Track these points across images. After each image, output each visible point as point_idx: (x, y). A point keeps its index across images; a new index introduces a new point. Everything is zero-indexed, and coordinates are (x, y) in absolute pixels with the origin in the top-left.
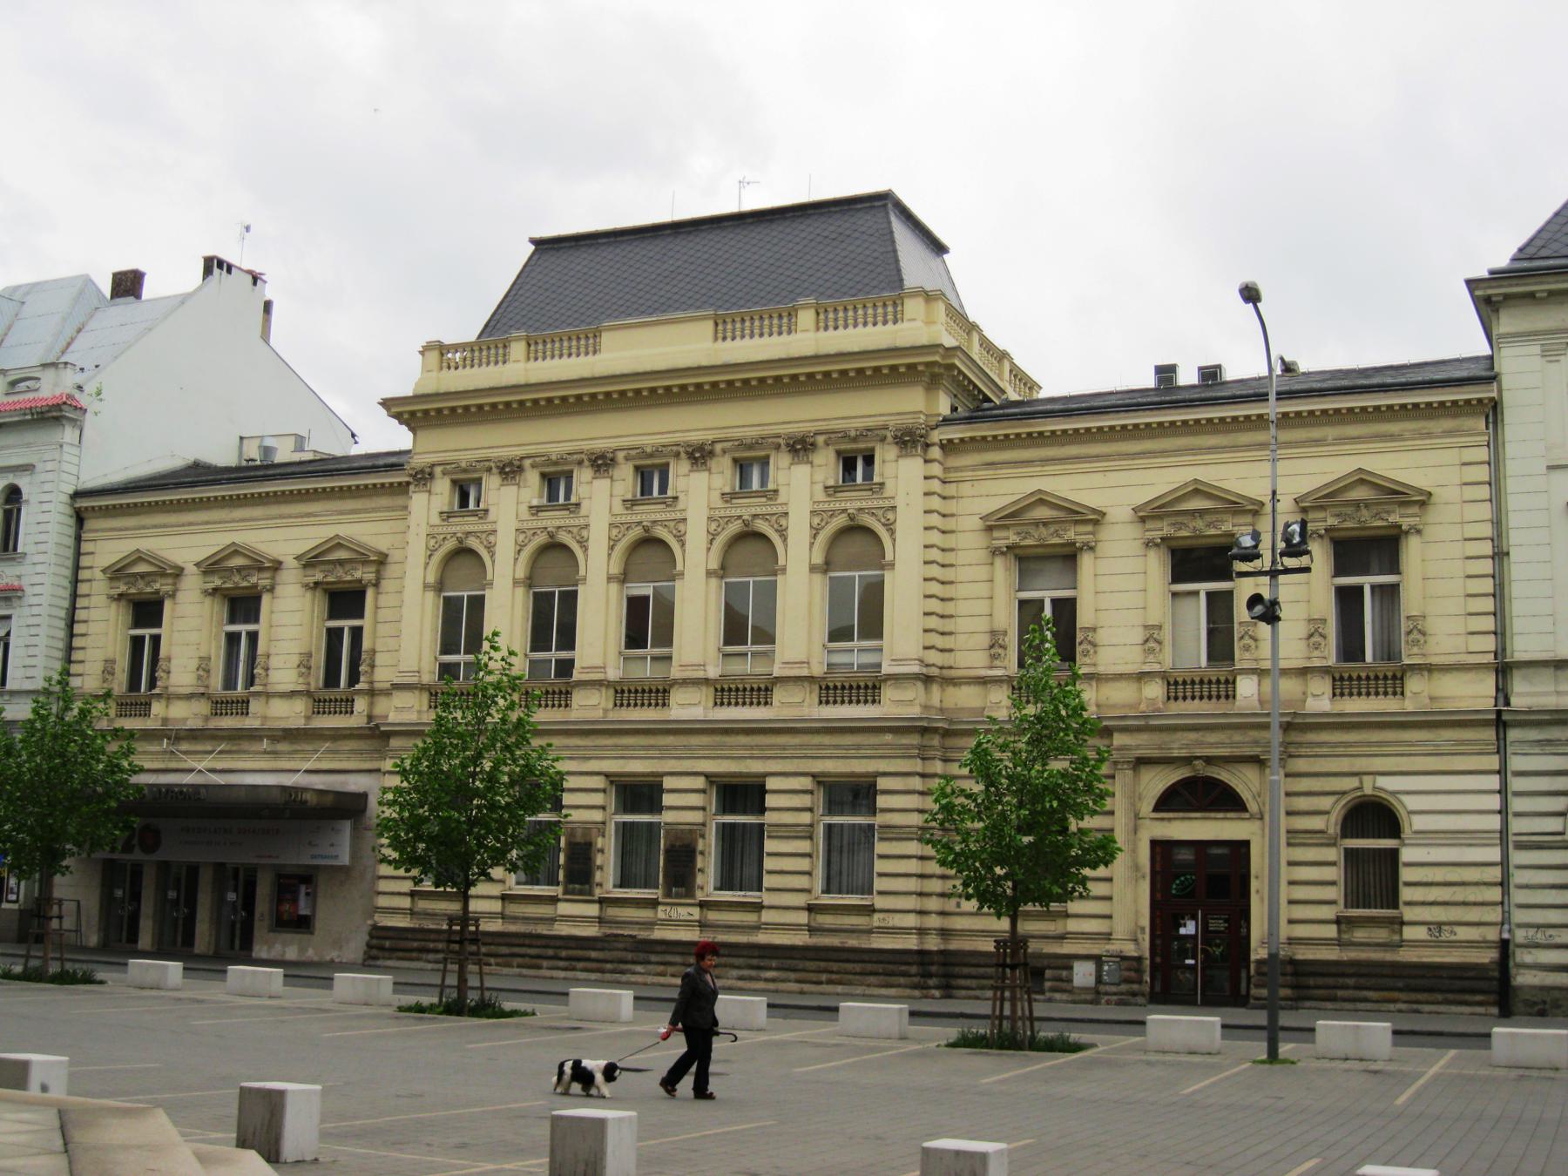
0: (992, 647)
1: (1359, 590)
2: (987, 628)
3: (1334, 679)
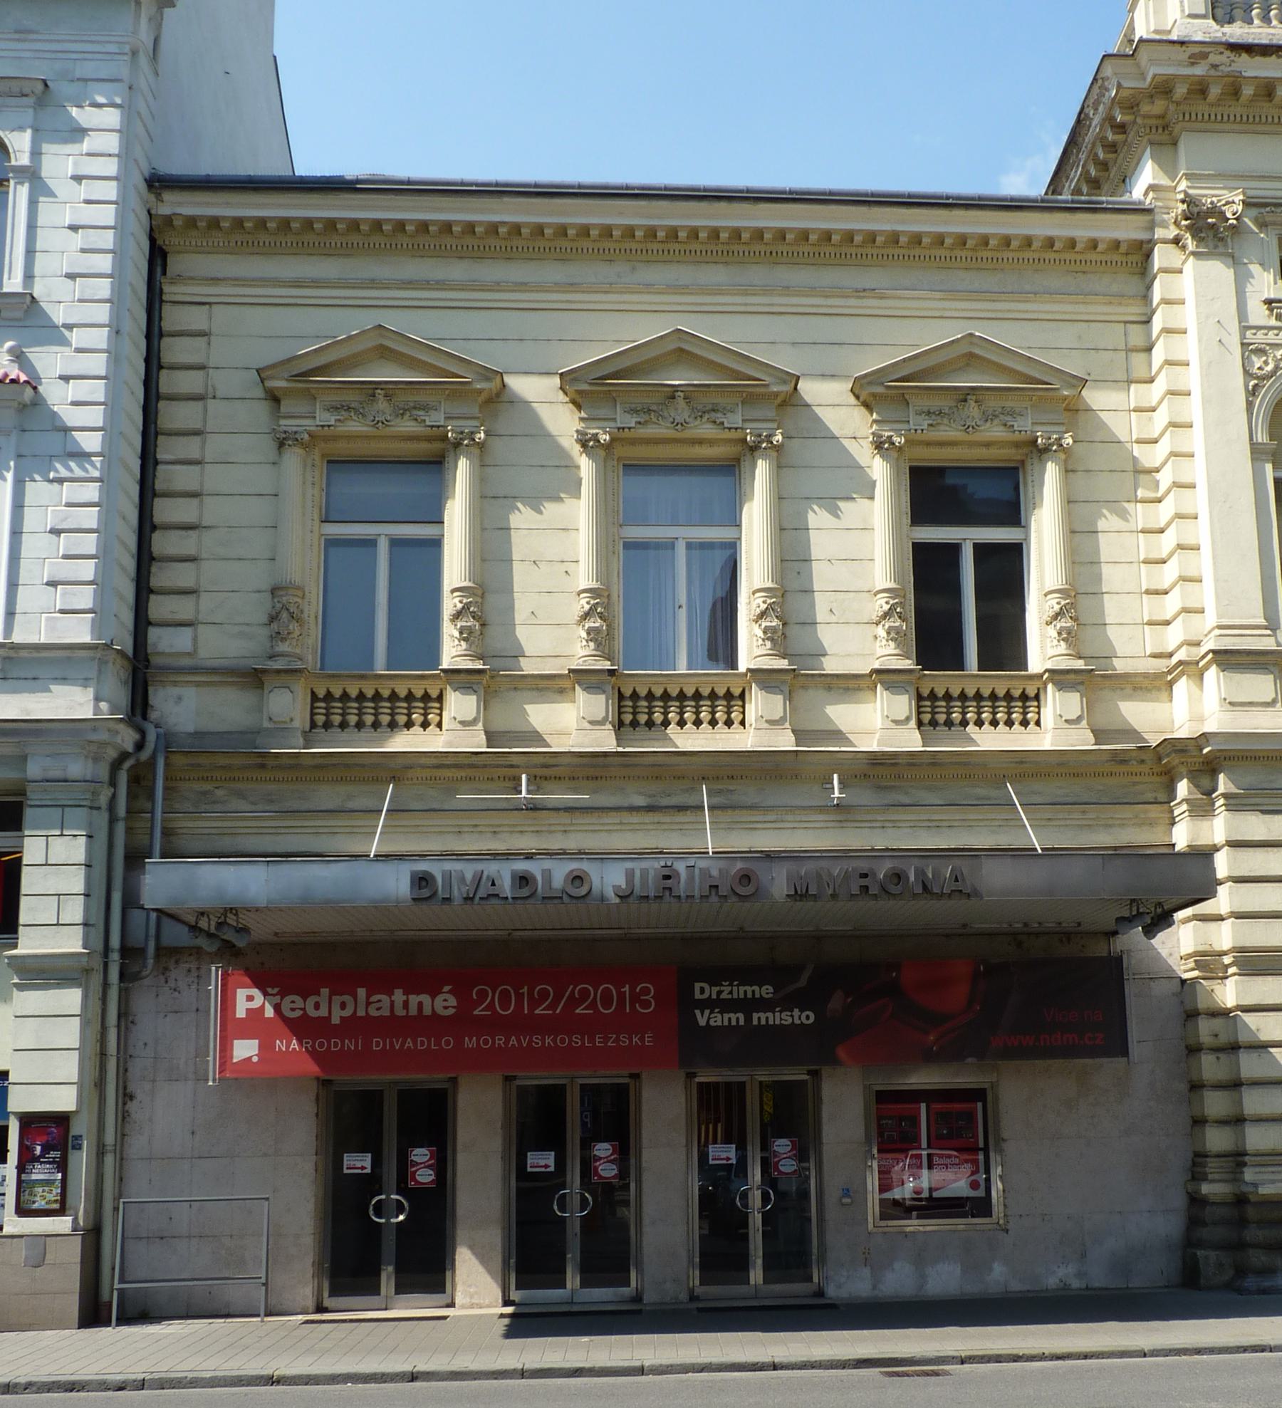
0: (273, 618)
1: (953, 550)
2: (266, 586)
3: (920, 698)
